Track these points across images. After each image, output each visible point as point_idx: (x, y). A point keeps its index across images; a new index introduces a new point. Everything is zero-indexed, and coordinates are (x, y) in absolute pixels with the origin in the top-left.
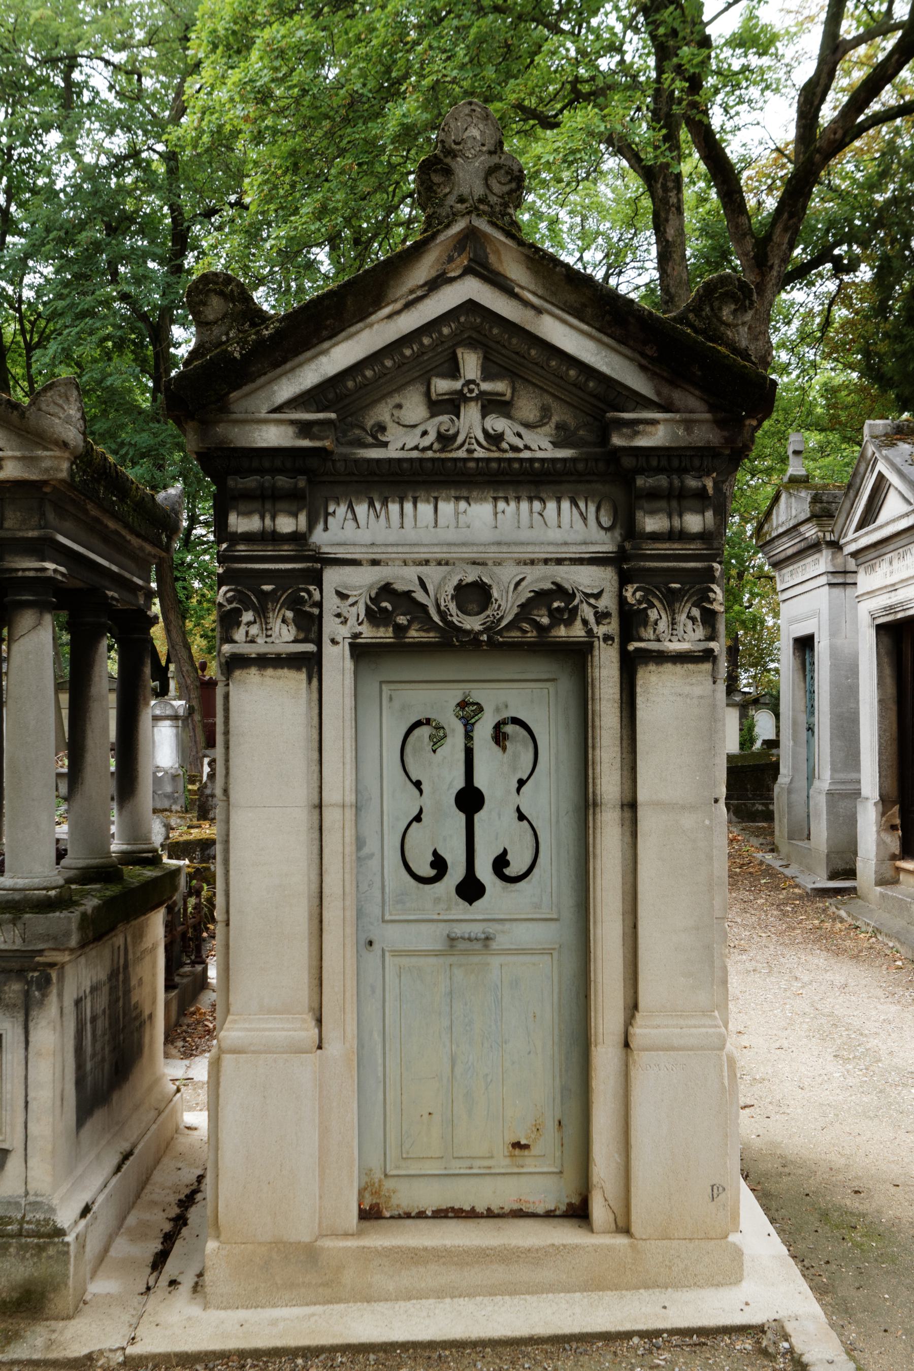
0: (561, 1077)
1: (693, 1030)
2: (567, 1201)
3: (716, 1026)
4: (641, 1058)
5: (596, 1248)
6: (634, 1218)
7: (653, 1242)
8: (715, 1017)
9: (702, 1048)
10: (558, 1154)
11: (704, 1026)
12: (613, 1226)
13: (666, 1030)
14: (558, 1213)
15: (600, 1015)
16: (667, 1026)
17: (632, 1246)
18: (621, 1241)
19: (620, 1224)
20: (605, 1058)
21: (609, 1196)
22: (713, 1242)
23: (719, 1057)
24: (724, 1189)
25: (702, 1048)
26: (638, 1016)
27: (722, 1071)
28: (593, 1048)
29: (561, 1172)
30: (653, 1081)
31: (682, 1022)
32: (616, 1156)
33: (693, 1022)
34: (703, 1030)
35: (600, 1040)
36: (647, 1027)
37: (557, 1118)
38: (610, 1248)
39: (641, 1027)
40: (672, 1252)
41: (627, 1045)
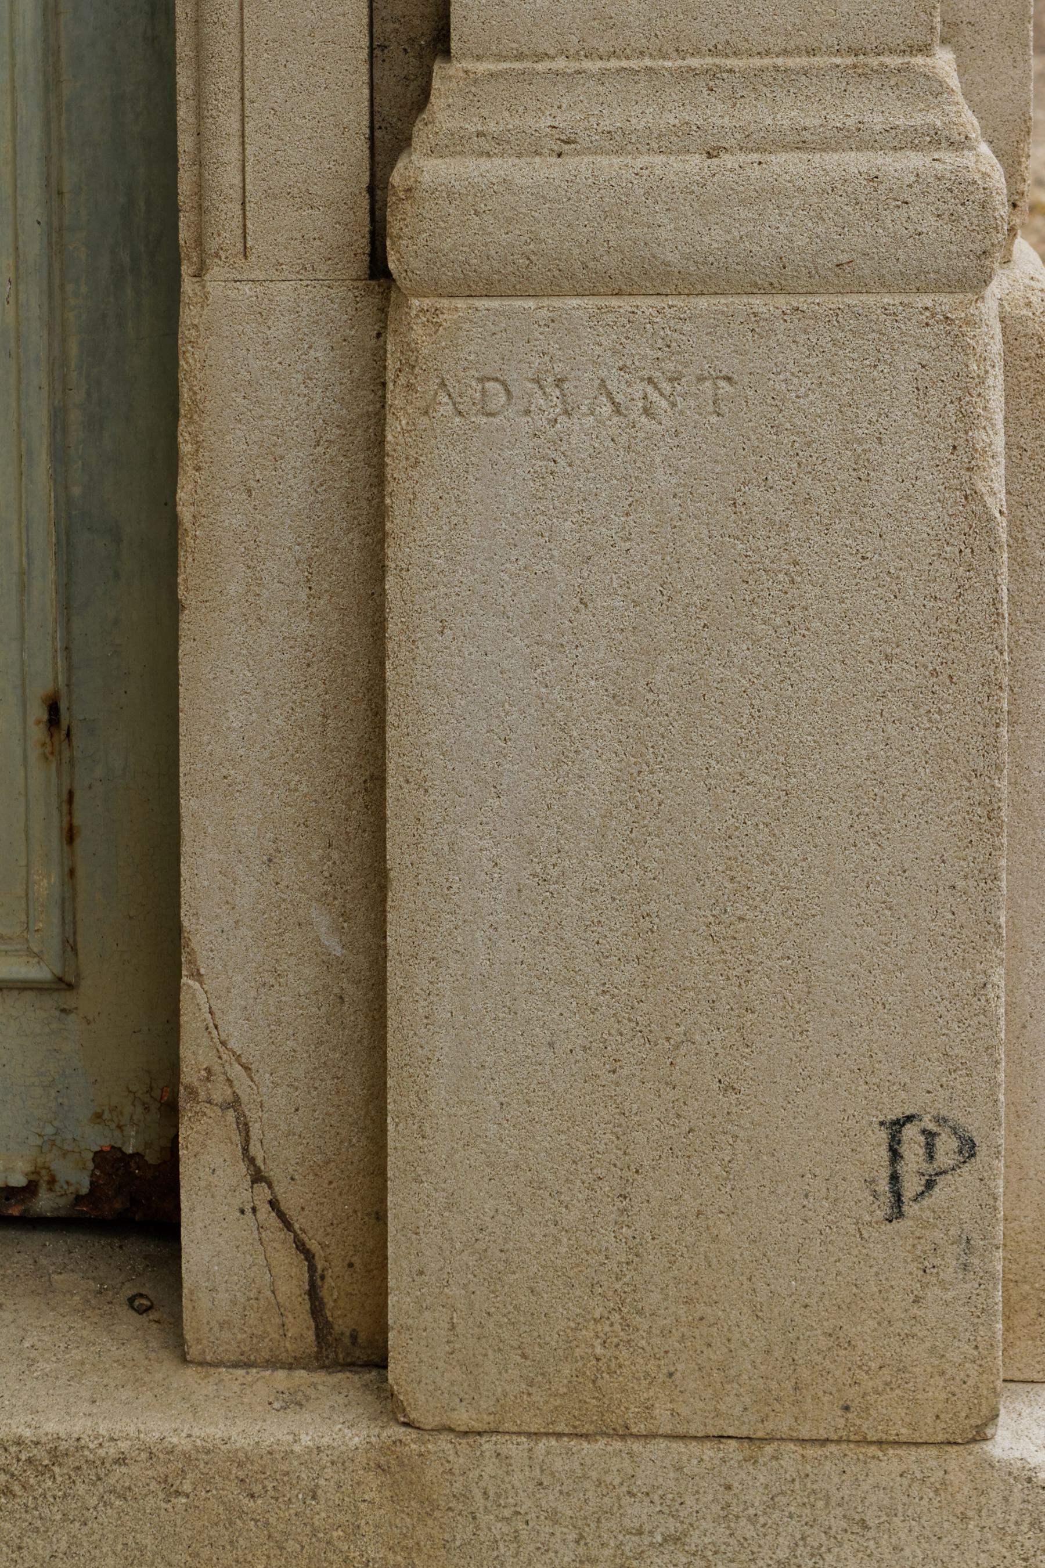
0: (59, 455)
1: (787, 164)
2: (97, 1139)
3: (937, 139)
4: (450, 336)
5: (175, 1473)
6: (399, 1304)
7: (516, 1449)
8: (938, 90)
9: (843, 276)
10: (46, 883)
11: (857, 138)
12: (301, 1327)
13: (609, 164)
14: (45, 1203)
15: (223, 83)
16: (619, 142)
17: (387, 1464)
18: (324, 1427)
19: (342, 1324)
20: (255, 333)
21: (281, 1157)
22: (891, 1464)
23: (957, 335)
24: (968, 1149)
25: (843, 276)
26: (446, 78)
27: (967, 419)
28: (188, 286)
29: (63, 984)
30: (532, 488)
31: (718, 115)
32: (321, 920)
33: (788, 114)
34: (855, 162)
35: (224, 233)
36: (496, 144)
37: (40, 688)
38: (255, 1475)
39: (456, 146)
40: (637, 1512)
41: (378, 268)
